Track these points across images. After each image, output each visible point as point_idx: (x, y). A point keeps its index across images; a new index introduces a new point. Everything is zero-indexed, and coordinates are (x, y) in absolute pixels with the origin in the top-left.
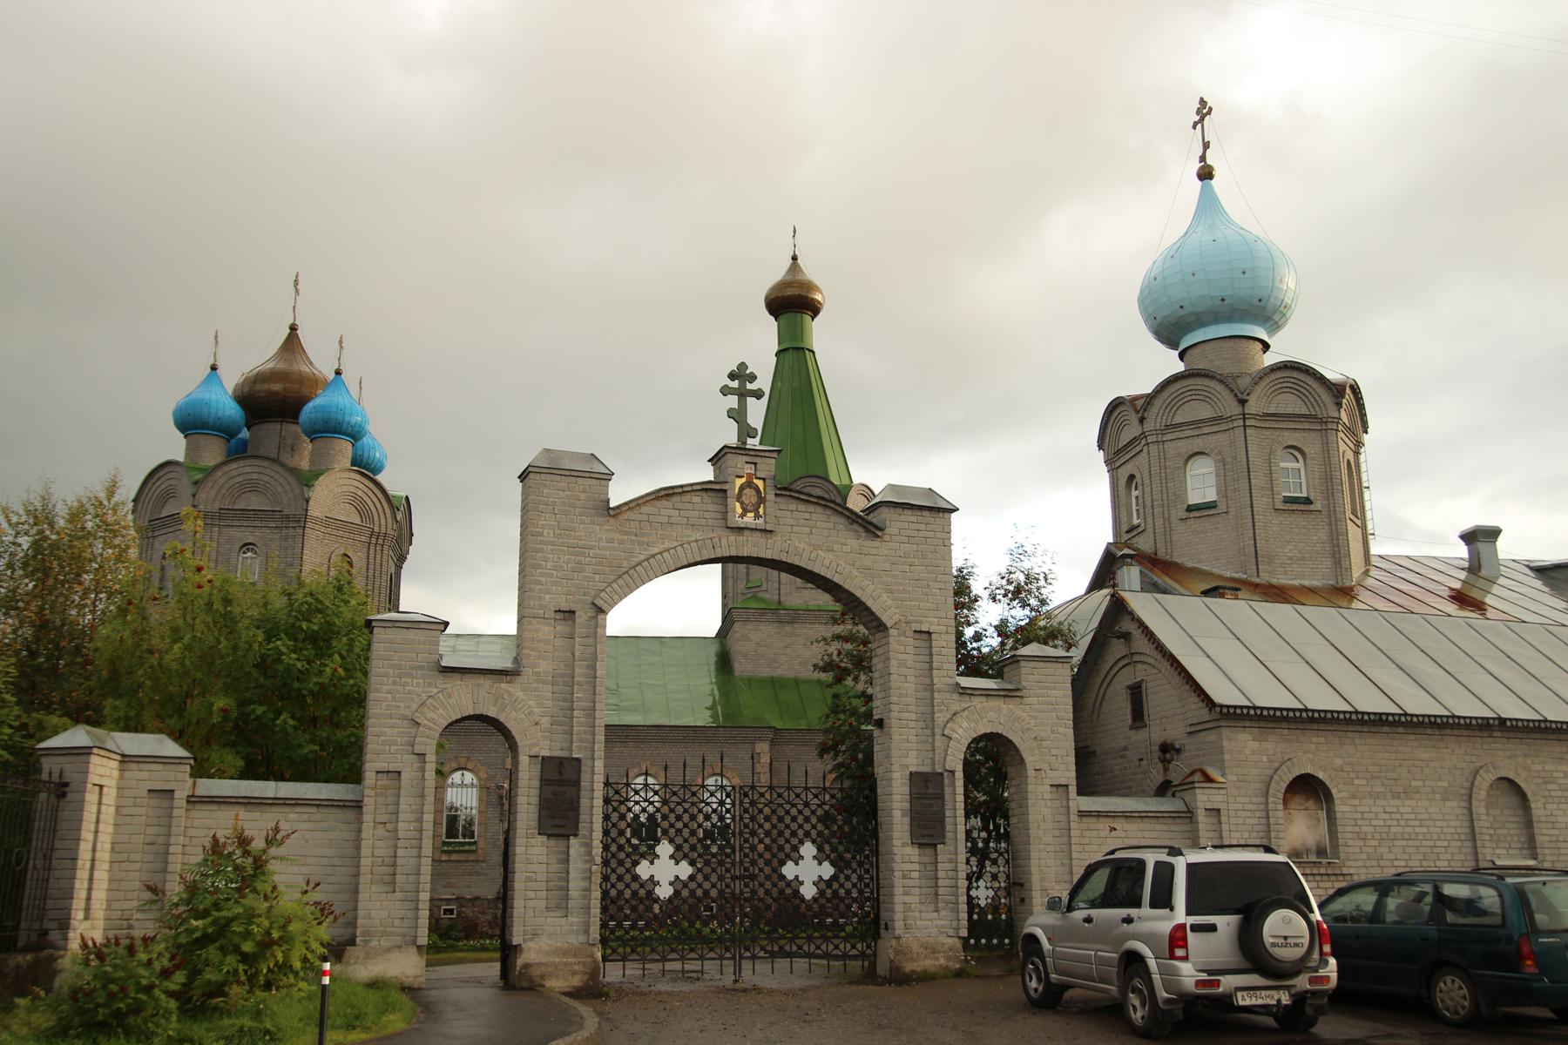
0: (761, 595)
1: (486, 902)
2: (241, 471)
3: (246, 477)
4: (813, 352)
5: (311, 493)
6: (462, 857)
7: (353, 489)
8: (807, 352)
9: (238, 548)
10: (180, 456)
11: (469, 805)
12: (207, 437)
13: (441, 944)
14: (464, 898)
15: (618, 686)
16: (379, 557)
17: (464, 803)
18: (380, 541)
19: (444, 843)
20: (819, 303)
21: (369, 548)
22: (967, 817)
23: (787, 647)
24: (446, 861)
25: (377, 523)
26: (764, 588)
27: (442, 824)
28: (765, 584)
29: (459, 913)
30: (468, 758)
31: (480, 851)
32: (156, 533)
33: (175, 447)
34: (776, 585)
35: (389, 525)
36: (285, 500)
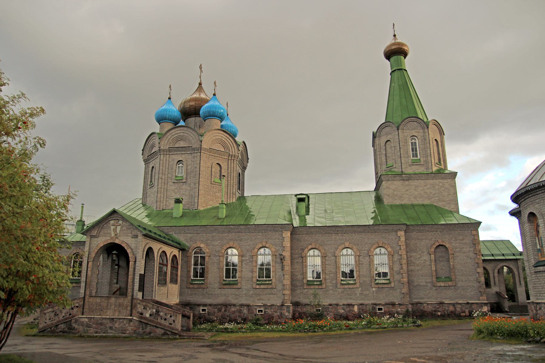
0: (393, 170)
1: (277, 307)
2: (176, 132)
3: (178, 135)
4: (406, 71)
5: (202, 138)
6: (266, 286)
7: (220, 138)
8: (404, 71)
9: (176, 163)
10: (158, 131)
12: (166, 123)
13: (253, 328)
14: (267, 305)
16: (232, 164)
18: (233, 158)
19: (257, 280)
20: (407, 50)
21: (228, 161)
23: (407, 190)
24: (258, 288)
25: (231, 151)
26: (394, 166)
27: (256, 272)
28: (394, 165)
29: (265, 312)
30: (267, 242)
31: (273, 284)
32: (150, 161)
34: (400, 164)
35: (236, 152)
36: (193, 142)
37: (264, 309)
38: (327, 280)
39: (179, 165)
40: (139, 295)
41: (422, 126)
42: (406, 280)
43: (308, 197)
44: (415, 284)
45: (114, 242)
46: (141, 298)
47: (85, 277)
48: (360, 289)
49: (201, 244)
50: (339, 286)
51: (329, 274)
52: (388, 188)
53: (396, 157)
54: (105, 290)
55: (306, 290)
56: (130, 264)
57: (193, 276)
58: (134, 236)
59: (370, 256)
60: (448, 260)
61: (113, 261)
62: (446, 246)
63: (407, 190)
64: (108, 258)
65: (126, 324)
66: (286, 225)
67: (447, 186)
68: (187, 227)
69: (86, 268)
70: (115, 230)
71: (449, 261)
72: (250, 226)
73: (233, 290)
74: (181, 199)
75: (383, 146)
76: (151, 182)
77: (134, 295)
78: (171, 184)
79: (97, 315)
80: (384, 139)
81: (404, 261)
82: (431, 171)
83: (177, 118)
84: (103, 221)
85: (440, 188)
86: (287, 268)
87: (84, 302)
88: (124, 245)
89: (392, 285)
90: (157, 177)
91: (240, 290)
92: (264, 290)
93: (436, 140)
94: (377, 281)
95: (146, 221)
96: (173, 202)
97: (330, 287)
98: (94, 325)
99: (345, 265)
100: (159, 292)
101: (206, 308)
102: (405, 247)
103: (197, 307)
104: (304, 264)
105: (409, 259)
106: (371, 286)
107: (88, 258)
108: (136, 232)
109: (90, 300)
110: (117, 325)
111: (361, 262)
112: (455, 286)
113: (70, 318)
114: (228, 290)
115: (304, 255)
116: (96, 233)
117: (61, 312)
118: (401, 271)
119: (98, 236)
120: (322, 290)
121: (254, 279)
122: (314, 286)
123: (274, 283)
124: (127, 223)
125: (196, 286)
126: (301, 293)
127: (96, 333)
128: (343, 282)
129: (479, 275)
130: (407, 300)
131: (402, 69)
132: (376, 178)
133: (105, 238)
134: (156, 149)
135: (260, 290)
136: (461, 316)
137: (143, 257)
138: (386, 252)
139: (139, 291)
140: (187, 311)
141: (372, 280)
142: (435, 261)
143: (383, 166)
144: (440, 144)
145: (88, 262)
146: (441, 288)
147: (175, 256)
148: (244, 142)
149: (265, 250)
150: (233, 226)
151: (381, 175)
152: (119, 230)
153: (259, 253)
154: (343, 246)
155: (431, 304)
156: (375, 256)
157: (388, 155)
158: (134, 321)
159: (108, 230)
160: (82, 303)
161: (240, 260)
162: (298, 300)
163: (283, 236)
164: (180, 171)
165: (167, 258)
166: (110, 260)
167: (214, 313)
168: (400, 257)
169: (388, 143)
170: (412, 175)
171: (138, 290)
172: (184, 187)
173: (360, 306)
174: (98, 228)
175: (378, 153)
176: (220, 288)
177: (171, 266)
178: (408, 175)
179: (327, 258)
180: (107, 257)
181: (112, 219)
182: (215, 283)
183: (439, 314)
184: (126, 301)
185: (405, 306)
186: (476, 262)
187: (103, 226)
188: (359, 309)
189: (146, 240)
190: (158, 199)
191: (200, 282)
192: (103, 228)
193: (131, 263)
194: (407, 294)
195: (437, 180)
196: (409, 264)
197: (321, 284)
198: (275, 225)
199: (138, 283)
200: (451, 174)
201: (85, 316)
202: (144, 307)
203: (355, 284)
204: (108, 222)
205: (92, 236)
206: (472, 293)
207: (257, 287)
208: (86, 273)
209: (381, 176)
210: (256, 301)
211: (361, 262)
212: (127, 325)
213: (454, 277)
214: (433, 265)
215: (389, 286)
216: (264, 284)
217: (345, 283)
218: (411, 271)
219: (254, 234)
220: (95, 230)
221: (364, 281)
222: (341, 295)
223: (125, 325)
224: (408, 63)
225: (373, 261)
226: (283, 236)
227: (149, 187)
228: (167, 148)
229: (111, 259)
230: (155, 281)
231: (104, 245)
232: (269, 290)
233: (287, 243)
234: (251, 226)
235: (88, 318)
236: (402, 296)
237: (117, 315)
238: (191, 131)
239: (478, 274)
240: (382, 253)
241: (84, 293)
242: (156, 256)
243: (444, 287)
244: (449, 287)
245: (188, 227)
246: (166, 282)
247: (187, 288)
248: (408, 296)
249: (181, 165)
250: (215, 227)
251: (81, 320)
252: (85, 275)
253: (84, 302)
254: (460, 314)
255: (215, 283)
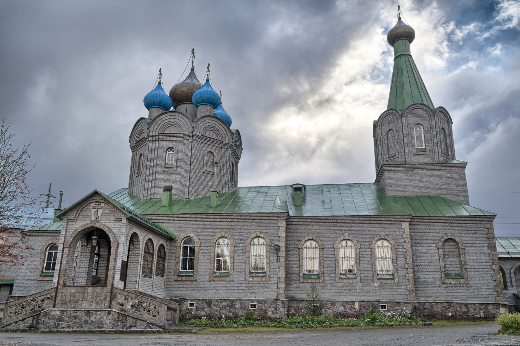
0: (396, 160)
2: (167, 118)
3: (169, 120)
6: (259, 279)
10: (147, 116)
11: (262, 254)
15: (331, 201)
17: (260, 254)
19: (251, 273)
22: (360, 302)
23: (411, 181)
31: (267, 276)
32: (138, 149)
33: (145, 113)
37: (257, 304)
38: (325, 274)
39: (169, 153)
40: (120, 285)
41: (428, 113)
42: (411, 275)
43: (305, 188)
44: (422, 280)
45: (94, 226)
46: (122, 288)
47: (59, 264)
48: (361, 284)
49: (191, 234)
50: (338, 279)
51: (328, 267)
52: (390, 178)
53: (399, 146)
54: (82, 280)
55: (303, 284)
56: (112, 251)
57: (181, 268)
58: (117, 220)
59: (372, 248)
60: (458, 255)
61: (93, 248)
62: (456, 240)
63: (411, 181)
64: (87, 246)
65: (103, 317)
66: (281, 214)
67: (455, 176)
68: (176, 215)
69: (61, 255)
70: (96, 213)
71: (460, 257)
72: (243, 215)
73: (224, 282)
74: (171, 187)
75: (385, 135)
76: (139, 170)
77: (115, 284)
78: (160, 172)
79: (71, 308)
80: (386, 128)
81: (409, 255)
82: (437, 161)
83: (167, 104)
84: (82, 203)
85: (447, 179)
86: (282, 259)
87: (56, 293)
88: (105, 229)
89: (396, 280)
90: (145, 165)
91: (232, 282)
92: (257, 283)
93: (443, 128)
94: (379, 276)
95: (132, 208)
96: (161, 190)
97: (328, 281)
98: (67, 319)
99: (345, 258)
100: (144, 283)
101: (194, 303)
102: (409, 240)
103: (185, 302)
104: (300, 256)
105: (414, 253)
106: (373, 281)
107: (64, 244)
108: (119, 215)
109: (63, 290)
110: (93, 318)
111: (362, 255)
112: (467, 284)
113: (40, 311)
114: (219, 282)
115: (300, 246)
116: (74, 216)
117: (29, 304)
118: (406, 265)
119: (77, 220)
120: (319, 284)
121: (247, 271)
122: (310, 280)
123: (268, 275)
124: (110, 205)
125: (184, 278)
126: (296, 287)
127: (69, 327)
128: (342, 276)
129: (494, 273)
130: (412, 298)
131: (407, 54)
132: (377, 169)
133: (85, 222)
134: (145, 135)
135: (253, 283)
136: (475, 318)
137: (126, 243)
138: (389, 245)
139: (120, 280)
140: (175, 306)
141: (373, 274)
142: (444, 257)
143: (384, 156)
144: (447, 133)
145: (63, 248)
146: (451, 285)
147: (162, 245)
148: (237, 131)
149: (259, 240)
150: (226, 215)
151: (382, 165)
152: (101, 213)
153: (252, 243)
154: (342, 238)
155: (441, 303)
156: (377, 249)
157: (390, 145)
158: (114, 312)
159: (88, 213)
160: (54, 293)
161: (233, 250)
162: (294, 295)
163: (279, 225)
164: (171, 158)
165: (153, 247)
166: (89, 248)
167: (203, 308)
168: (404, 251)
169: (391, 132)
170: (417, 165)
171: (119, 278)
172: (174, 175)
173: (362, 303)
174: (76, 211)
175: (379, 143)
176: (210, 281)
177: (158, 256)
178: (412, 165)
179: (325, 250)
180: (86, 245)
181: (93, 201)
182: (204, 275)
183: (450, 314)
184: (106, 291)
185: (411, 304)
186: (491, 258)
187: (83, 208)
188: (360, 306)
189: (130, 224)
190: (146, 188)
191: (189, 275)
192: (82, 211)
193: (113, 249)
194: (413, 291)
195: (445, 171)
196: (415, 259)
197: (318, 278)
198: (270, 214)
199: (120, 270)
200: (460, 164)
201: (57, 309)
202: (126, 297)
203: (355, 278)
204: (88, 205)
205: (68, 220)
206: (488, 292)
207: (251, 279)
208: (60, 261)
209: (383, 166)
210: (249, 295)
211: (362, 255)
212: (105, 318)
213: (465, 275)
214: (442, 260)
215: (393, 281)
216: (257, 277)
217: (344, 277)
218: (417, 266)
219: (248, 223)
220: (73, 213)
221: (365, 276)
222: (340, 290)
223: (102, 317)
224: (414, 48)
225: (375, 254)
226: (279, 225)
227: (136, 175)
228: (157, 134)
229: (90, 247)
230: (139, 270)
231: (83, 230)
232: (263, 283)
233: (282, 233)
234: (245, 215)
235: (60, 310)
236: (408, 293)
237: (94, 307)
238: (182, 116)
239: (493, 271)
240: (384, 246)
241: (57, 283)
242: (141, 243)
243: (455, 285)
244: (460, 285)
245: (178, 215)
246: (151, 273)
247: (175, 281)
248: (414, 294)
249: (171, 152)
250: (207, 215)
251: (52, 313)
252: (60, 262)
253: (56, 293)
254: (473, 315)
255: (204, 275)
